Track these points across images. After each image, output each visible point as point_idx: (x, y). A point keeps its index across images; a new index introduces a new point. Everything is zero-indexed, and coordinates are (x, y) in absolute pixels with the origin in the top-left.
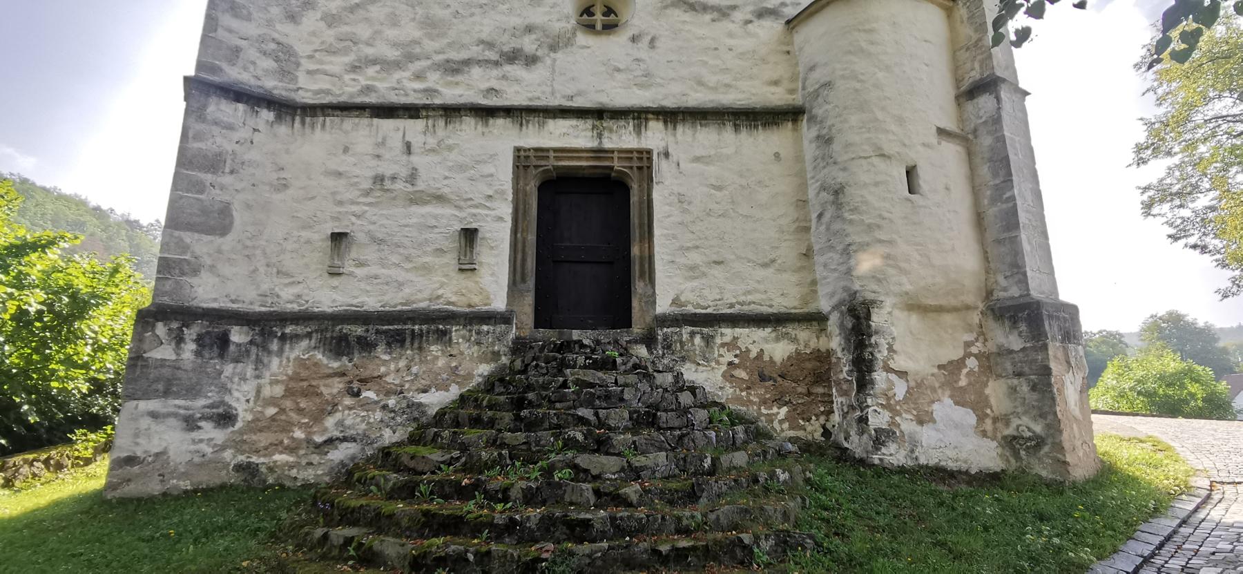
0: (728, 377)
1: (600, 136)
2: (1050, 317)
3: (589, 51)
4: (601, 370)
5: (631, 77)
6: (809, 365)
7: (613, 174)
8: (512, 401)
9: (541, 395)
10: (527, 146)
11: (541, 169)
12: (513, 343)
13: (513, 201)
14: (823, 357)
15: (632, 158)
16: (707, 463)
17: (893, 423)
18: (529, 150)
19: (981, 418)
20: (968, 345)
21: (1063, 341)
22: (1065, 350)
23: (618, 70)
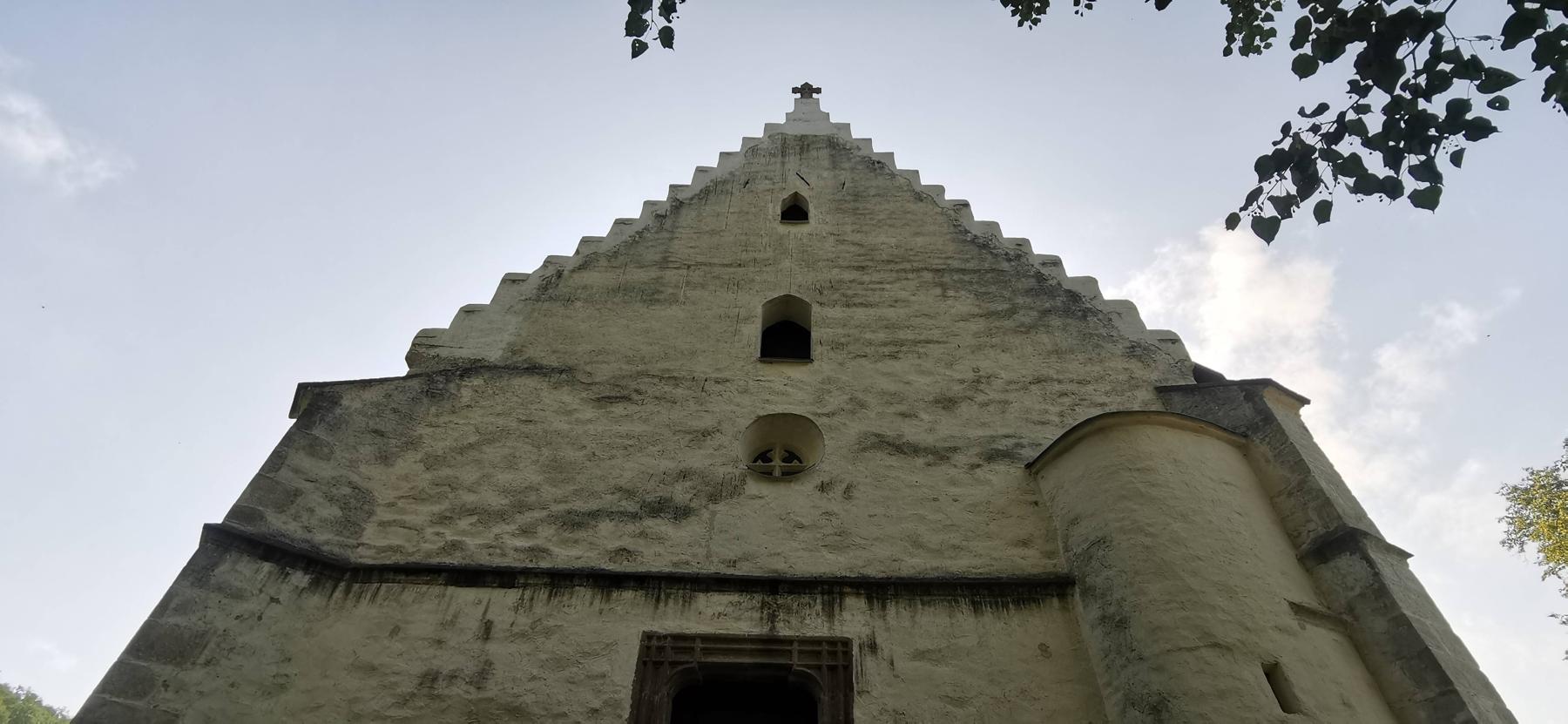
3: (763, 501)
5: (819, 536)
10: (662, 631)
11: (680, 668)
15: (819, 653)
18: (665, 637)
23: (801, 527)
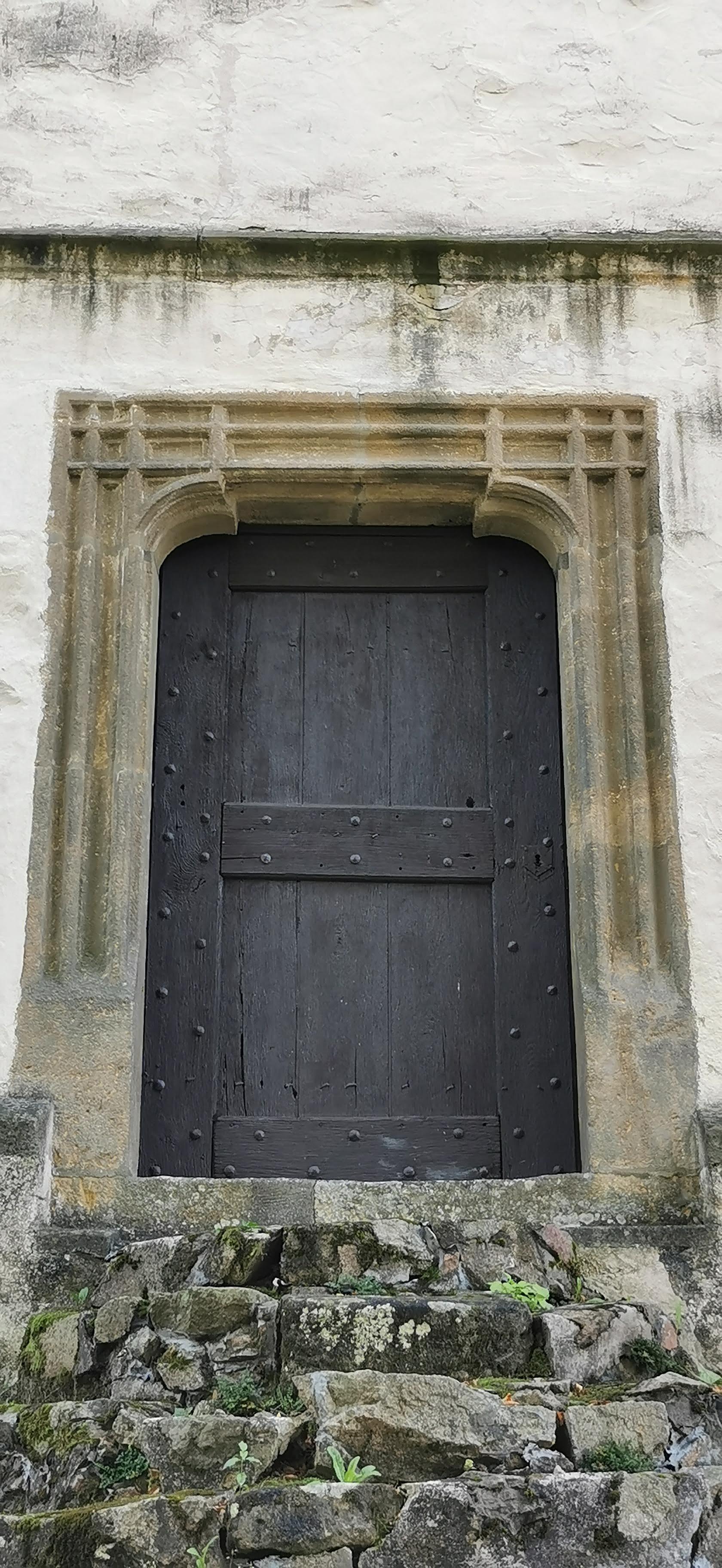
4: (475, 1371)
7: (485, 507)
8: (27, 1547)
9: (182, 1516)
10: (114, 391)
11: (175, 484)
12: (43, 1242)
13: (50, 616)
15: (563, 438)
18: (124, 406)
23: (499, 89)
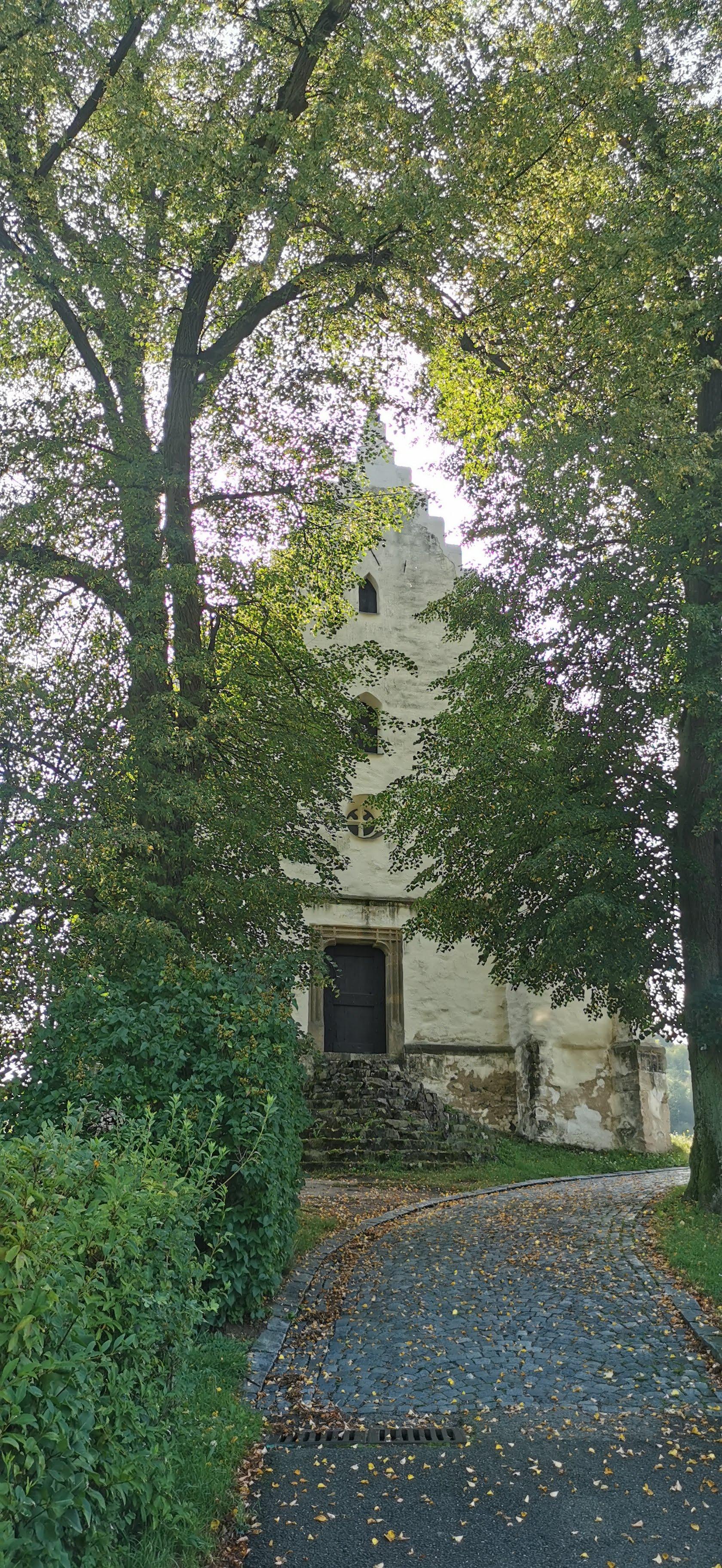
0: (451, 1087)
1: (367, 918)
2: (642, 1055)
6: (502, 1082)
14: (511, 1077)
16: (447, 1127)
17: (550, 1118)
19: (604, 1118)
20: (599, 1071)
21: (651, 1070)
22: (652, 1077)
23: (379, 869)
